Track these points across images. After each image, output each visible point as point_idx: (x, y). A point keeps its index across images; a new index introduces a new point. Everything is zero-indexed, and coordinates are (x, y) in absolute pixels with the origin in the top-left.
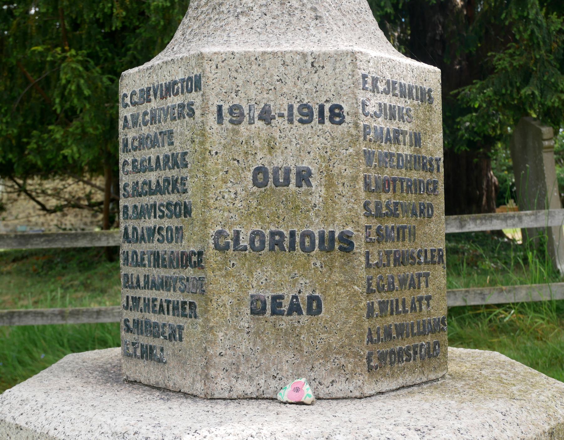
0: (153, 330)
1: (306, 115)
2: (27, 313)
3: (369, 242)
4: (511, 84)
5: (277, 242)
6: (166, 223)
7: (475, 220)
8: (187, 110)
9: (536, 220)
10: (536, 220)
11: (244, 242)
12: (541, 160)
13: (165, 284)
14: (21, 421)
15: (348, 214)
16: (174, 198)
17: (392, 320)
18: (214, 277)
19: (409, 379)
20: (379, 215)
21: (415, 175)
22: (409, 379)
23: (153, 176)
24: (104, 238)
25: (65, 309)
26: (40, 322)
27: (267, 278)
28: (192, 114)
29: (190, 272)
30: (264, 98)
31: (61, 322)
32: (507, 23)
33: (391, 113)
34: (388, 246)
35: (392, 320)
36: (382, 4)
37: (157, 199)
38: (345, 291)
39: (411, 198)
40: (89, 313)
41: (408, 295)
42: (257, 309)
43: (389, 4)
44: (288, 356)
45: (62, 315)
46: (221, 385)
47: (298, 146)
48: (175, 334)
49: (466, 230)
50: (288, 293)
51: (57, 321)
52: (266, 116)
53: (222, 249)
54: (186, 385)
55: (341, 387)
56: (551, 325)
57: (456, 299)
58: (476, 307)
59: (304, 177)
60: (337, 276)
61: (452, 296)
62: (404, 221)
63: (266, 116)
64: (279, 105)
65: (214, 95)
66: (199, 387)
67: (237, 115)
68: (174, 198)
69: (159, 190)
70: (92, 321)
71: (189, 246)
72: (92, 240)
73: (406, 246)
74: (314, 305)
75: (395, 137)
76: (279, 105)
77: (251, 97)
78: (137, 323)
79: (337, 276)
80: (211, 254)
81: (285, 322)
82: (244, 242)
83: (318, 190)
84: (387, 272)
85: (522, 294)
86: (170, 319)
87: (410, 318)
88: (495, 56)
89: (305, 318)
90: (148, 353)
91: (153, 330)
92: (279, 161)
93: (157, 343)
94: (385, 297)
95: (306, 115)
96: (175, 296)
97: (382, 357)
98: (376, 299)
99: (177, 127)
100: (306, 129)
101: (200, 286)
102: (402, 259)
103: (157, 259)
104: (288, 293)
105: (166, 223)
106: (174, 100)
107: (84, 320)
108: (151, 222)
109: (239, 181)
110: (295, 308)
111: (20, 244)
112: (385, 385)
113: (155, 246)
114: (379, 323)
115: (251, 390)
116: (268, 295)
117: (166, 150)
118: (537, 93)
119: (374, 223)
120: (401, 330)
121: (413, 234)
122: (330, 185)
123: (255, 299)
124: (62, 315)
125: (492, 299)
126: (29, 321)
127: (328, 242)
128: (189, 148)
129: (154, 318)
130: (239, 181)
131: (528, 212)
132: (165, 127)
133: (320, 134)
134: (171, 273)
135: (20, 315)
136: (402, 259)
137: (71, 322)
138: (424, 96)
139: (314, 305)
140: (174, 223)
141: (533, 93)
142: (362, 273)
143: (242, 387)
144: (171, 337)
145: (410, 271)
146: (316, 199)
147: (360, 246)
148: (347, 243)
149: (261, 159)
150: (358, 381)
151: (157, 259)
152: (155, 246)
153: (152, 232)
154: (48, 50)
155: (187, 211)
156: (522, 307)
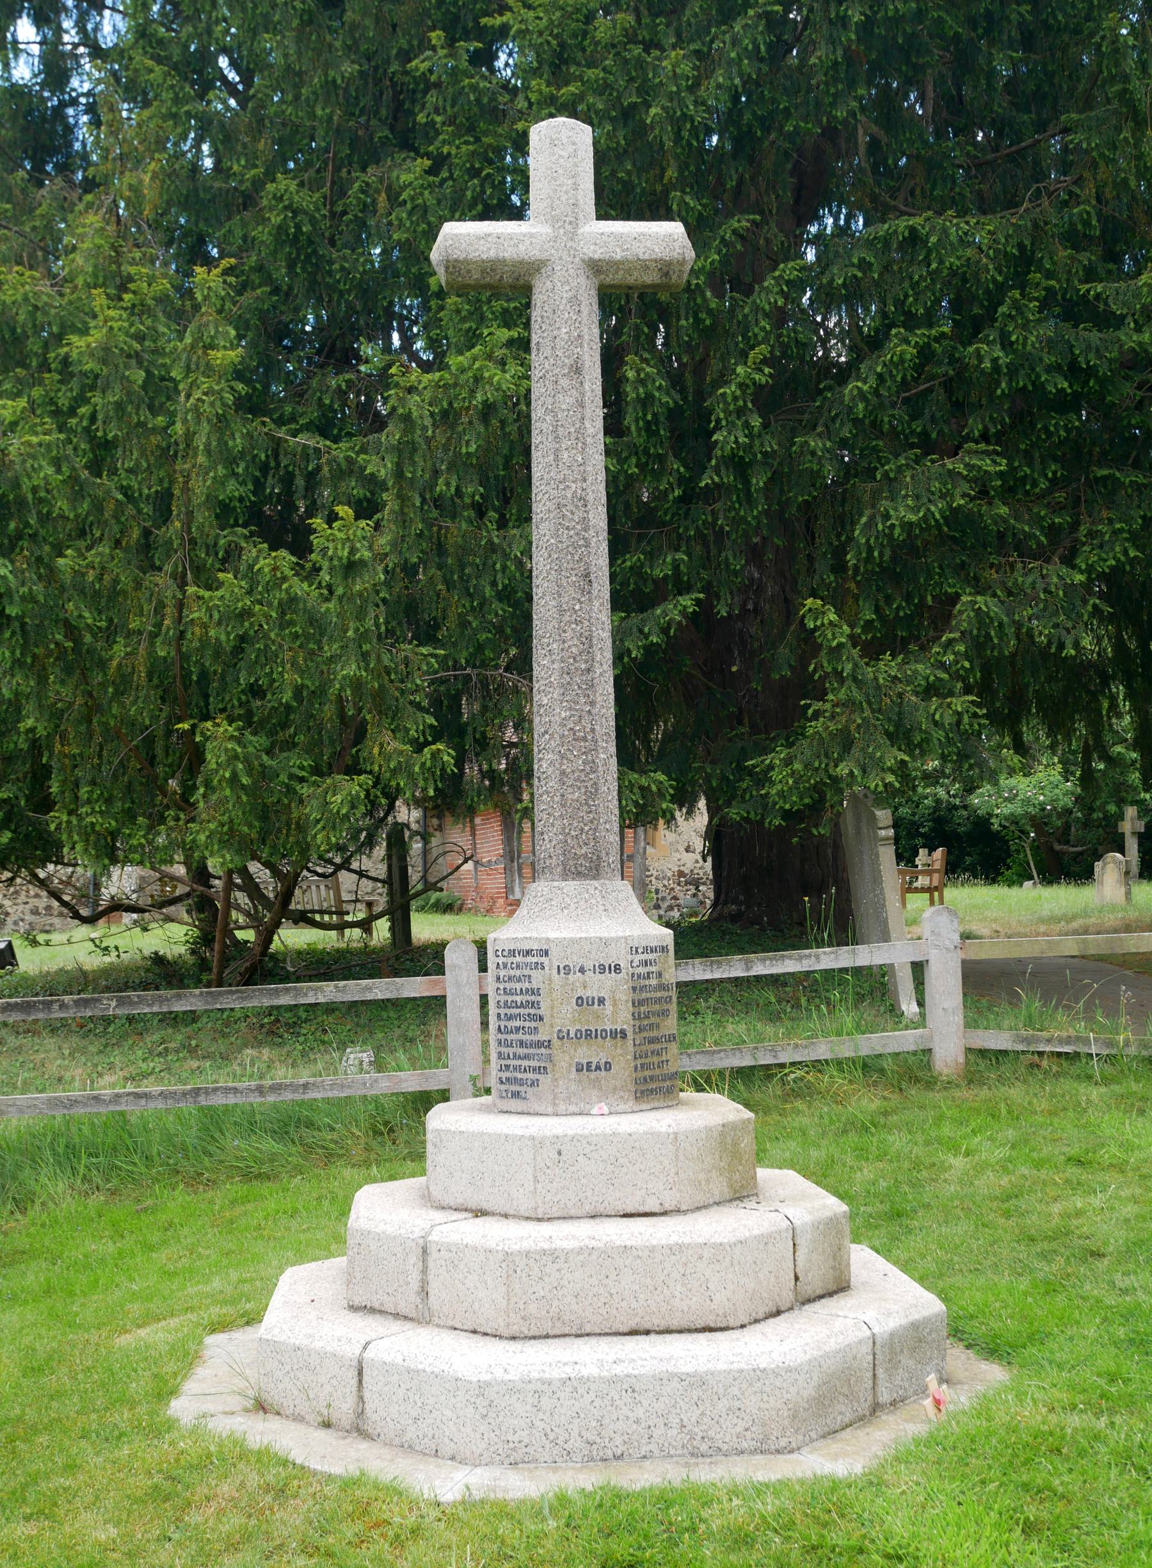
0: (521, 1082)
1: (602, 969)
2: (216, 1090)
3: (635, 1033)
4: (826, 756)
5: (588, 1034)
6: (527, 1024)
7: (763, 960)
8: (540, 966)
9: (836, 959)
10: (836, 959)
11: (572, 1035)
12: (877, 855)
13: (526, 1057)
14: (463, 1129)
15: (621, 1017)
16: (533, 1011)
17: (647, 1073)
18: (555, 1051)
19: (657, 1104)
20: (640, 1018)
21: (659, 994)
22: (657, 1104)
23: (518, 999)
24: (311, 993)
25: (263, 1082)
26: (232, 1100)
27: (585, 1053)
28: (543, 968)
29: (543, 1050)
30: (581, 961)
31: (259, 1100)
32: (816, 677)
33: (646, 963)
34: (645, 1034)
35: (647, 1073)
36: (646, 630)
37: (522, 1011)
38: (623, 1058)
39: (657, 1007)
40: (293, 1087)
41: (655, 1059)
42: (579, 1069)
43: (656, 629)
44: (595, 1092)
45: (260, 1090)
46: (562, 1107)
47: (597, 985)
48: (534, 1083)
49: (752, 973)
50: (595, 1061)
51: (255, 1099)
52: (582, 970)
53: (561, 1038)
54: (541, 1110)
55: (622, 1107)
56: (854, 1086)
57: (742, 1057)
58: (767, 1067)
59: (601, 1001)
60: (619, 1051)
61: (738, 1054)
62: (653, 1020)
63: (582, 970)
64: (589, 965)
65: (556, 958)
66: (550, 1110)
67: (567, 970)
68: (533, 1011)
69: (522, 1006)
70: (298, 1097)
71: (542, 1036)
72: (296, 996)
73: (655, 1033)
74: (608, 1066)
75: (648, 976)
76: (589, 965)
77: (574, 961)
78: (508, 1079)
79: (619, 1051)
80: (555, 1041)
81: (593, 1075)
82: (572, 1035)
83: (609, 1007)
84: (644, 1048)
85: (822, 1050)
86: (531, 1076)
87: (657, 1072)
88: (810, 706)
89: (603, 1073)
90: (516, 1095)
91: (521, 1082)
92: (589, 993)
93: (522, 1089)
94: (643, 1061)
95: (602, 969)
96: (534, 1063)
97: (642, 1092)
98: (639, 1062)
99: (534, 974)
100: (602, 976)
101: (550, 1058)
102: (652, 1041)
103: (522, 1044)
104: (595, 1061)
105: (527, 1024)
106: (529, 959)
107: (288, 1096)
108: (518, 1023)
109: (569, 1003)
110: (598, 1068)
111: (207, 1003)
112: (644, 1107)
113: (520, 1036)
114: (640, 1074)
115: (577, 1110)
116: (585, 1062)
117: (527, 985)
118: (856, 772)
119: (637, 1023)
120: (652, 1078)
121: (658, 1026)
122: (615, 1005)
123: (578, 1064)
124: (260, 1090)
125: (785, 1058)
126: (219, 1100)
127: (614, 1034)
128: (541, 986)
129: (519, 1076)
130: (569, 1003)
131: (827, 950)
132: (526, 972)
133: (610, 979)
134: (532, 1051)
135: (207, 1092)
136: (652, 1041)
137: (271, 1098)
138: (664, 949)
139: (608, 1066)
140: (533, 1024)
141: (851, 772)
142: (631, 1049)
143: (572, 1108)
144: (532, 1085)
145: (657, 1047)
146: (608, 1012)
147: (630, 1035)
148: (624, 1035)
149: (580, 992)
150: (631, 1104)
151: (522, 1044)
152: (520, 1036)
153: (518, 1029)
154: (194, 726)
155: (541, 1019)
156: (818, 1065)
